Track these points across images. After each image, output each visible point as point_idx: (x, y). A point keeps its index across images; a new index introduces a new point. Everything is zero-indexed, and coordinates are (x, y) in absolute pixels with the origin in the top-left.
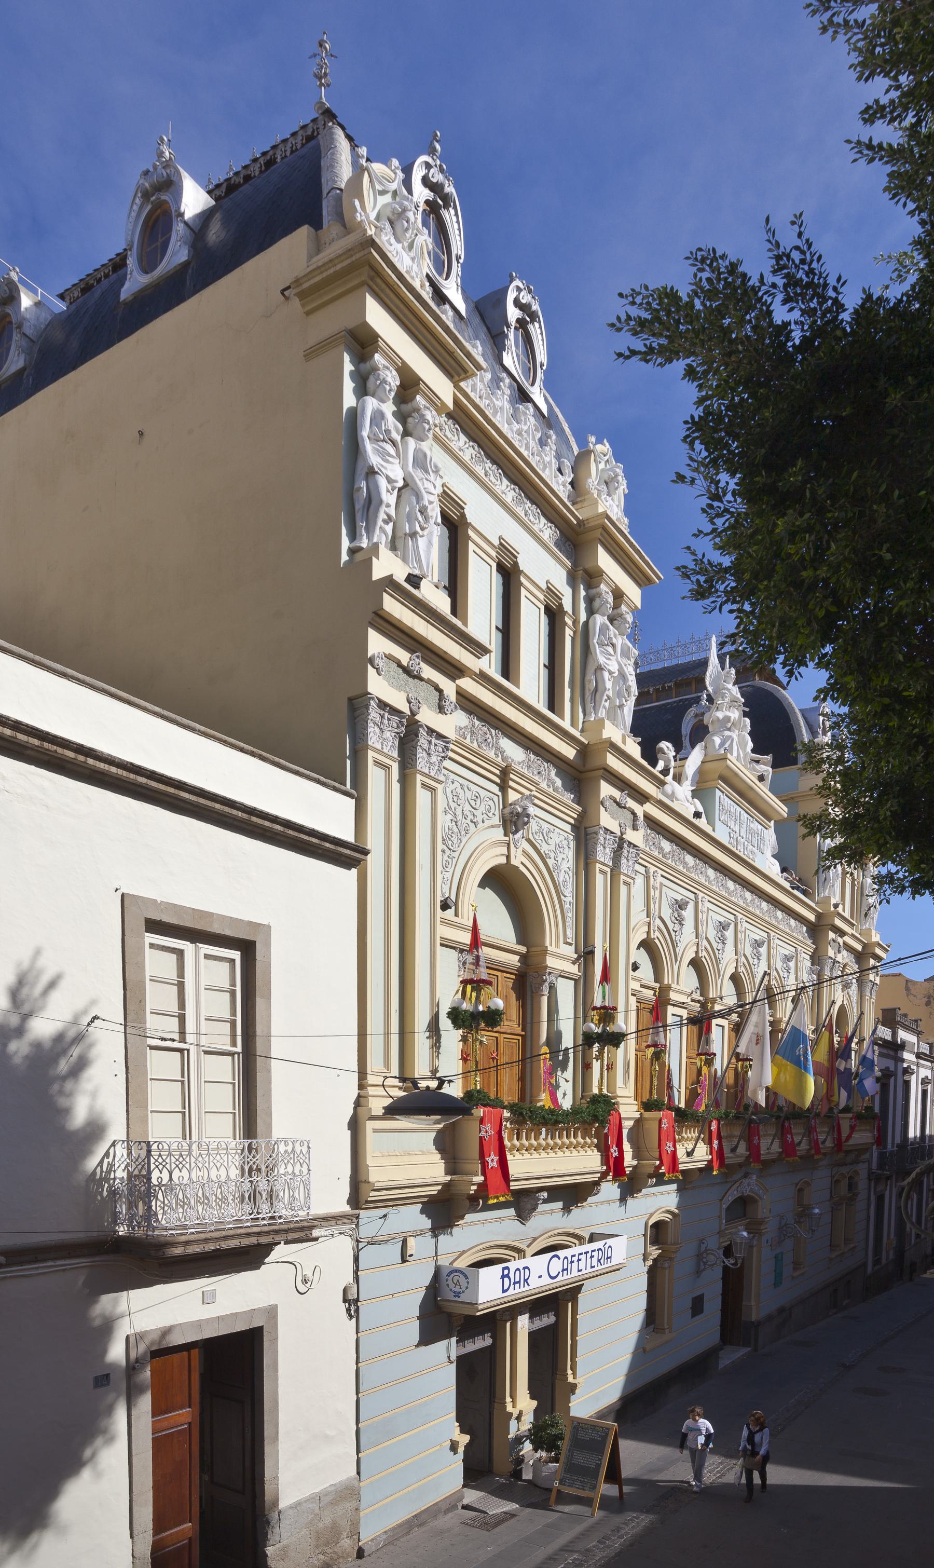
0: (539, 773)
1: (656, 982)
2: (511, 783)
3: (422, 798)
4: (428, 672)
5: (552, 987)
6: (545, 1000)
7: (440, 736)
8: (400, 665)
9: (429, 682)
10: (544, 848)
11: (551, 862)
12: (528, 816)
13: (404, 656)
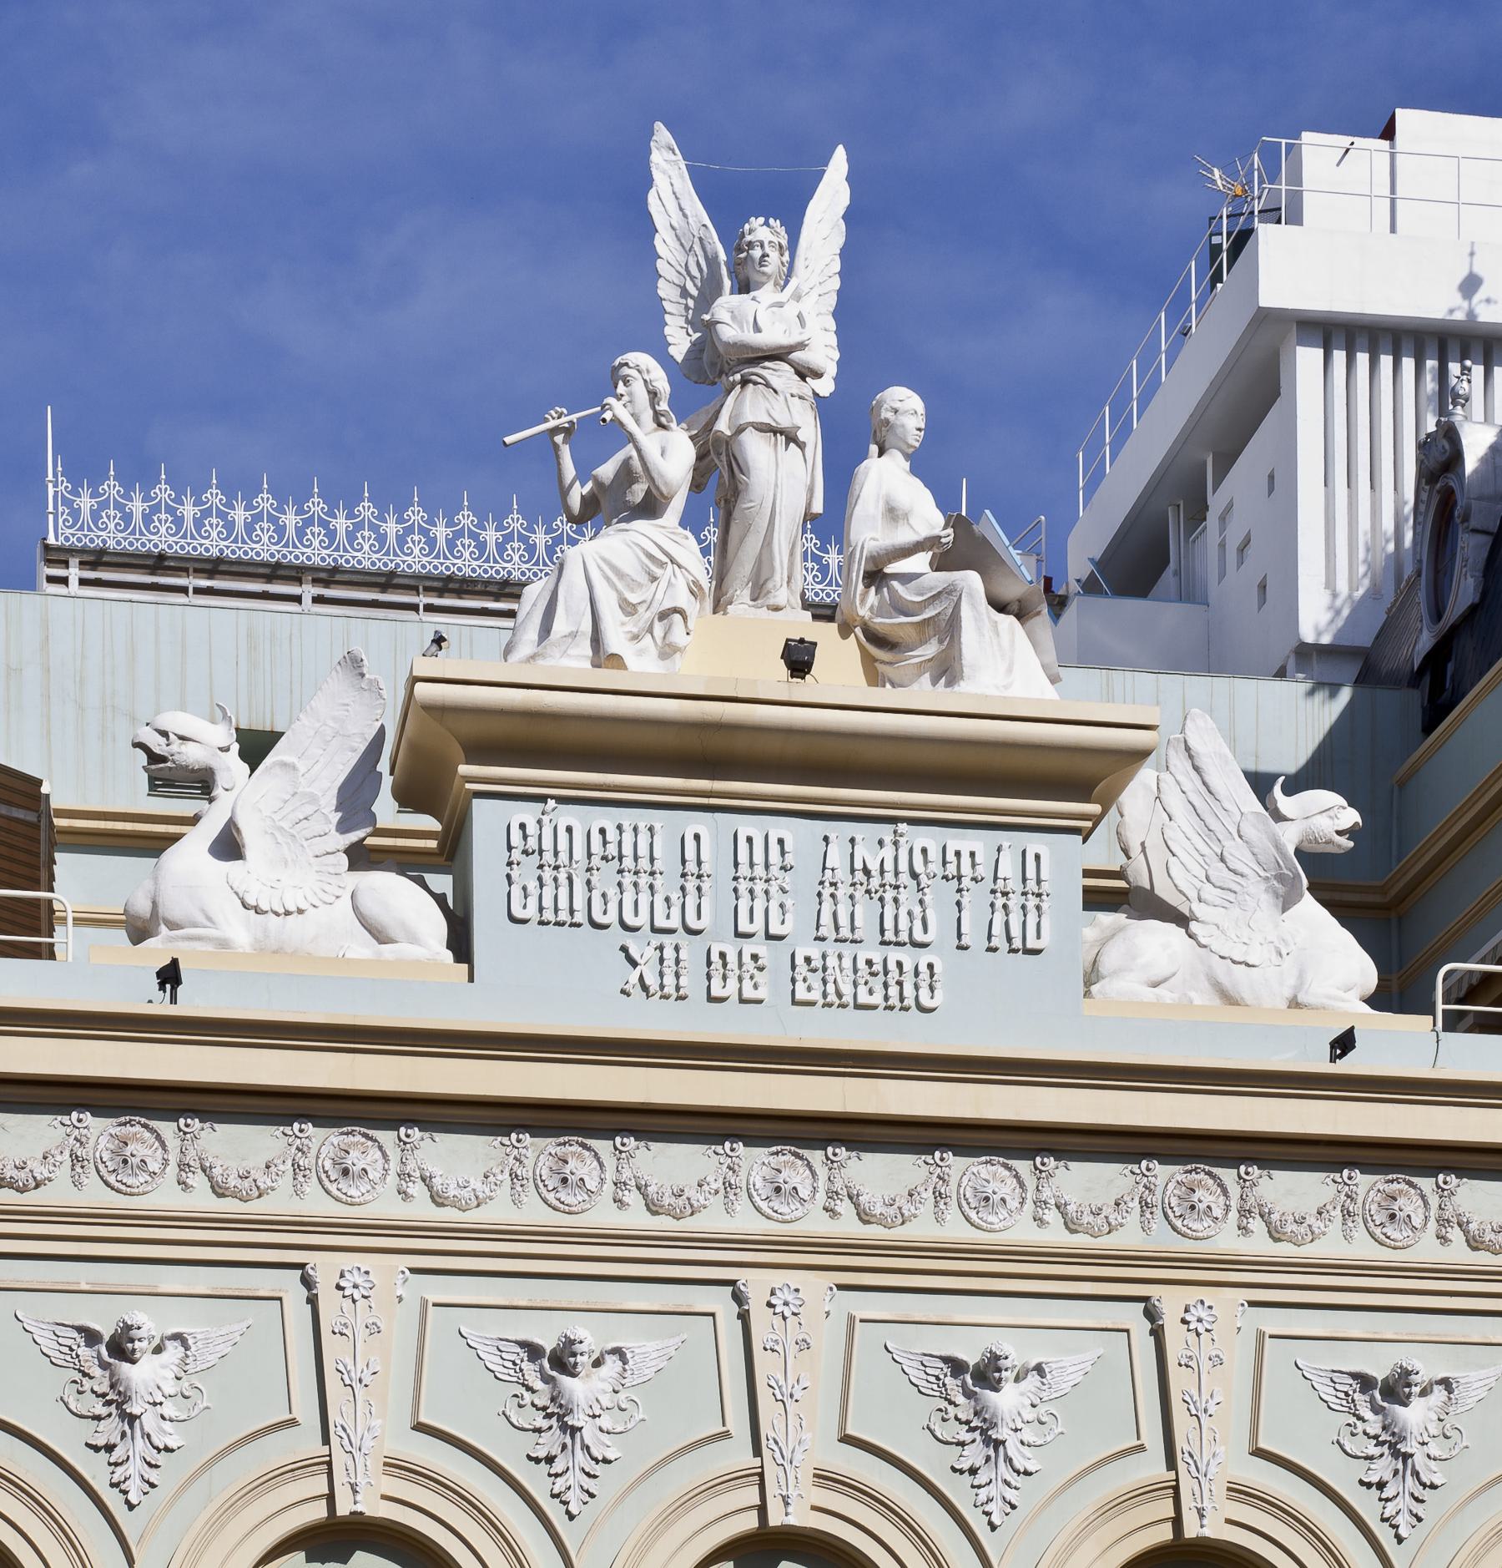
0: (345, 1172)
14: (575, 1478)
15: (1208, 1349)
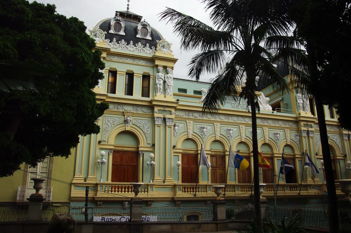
1: (272, 152)
2: (125, 114)
3: (311, 140)
4: (167, 109)
5: (339, 162)
6: (141, 158)
7: (312, 131)
8: (162, 110)
9: (168, 111)
10: (334, 140)
11: (335, 142)
12: (128, 120)
13: (162, 109)
14: (175, 134)
15: (266, 131)
